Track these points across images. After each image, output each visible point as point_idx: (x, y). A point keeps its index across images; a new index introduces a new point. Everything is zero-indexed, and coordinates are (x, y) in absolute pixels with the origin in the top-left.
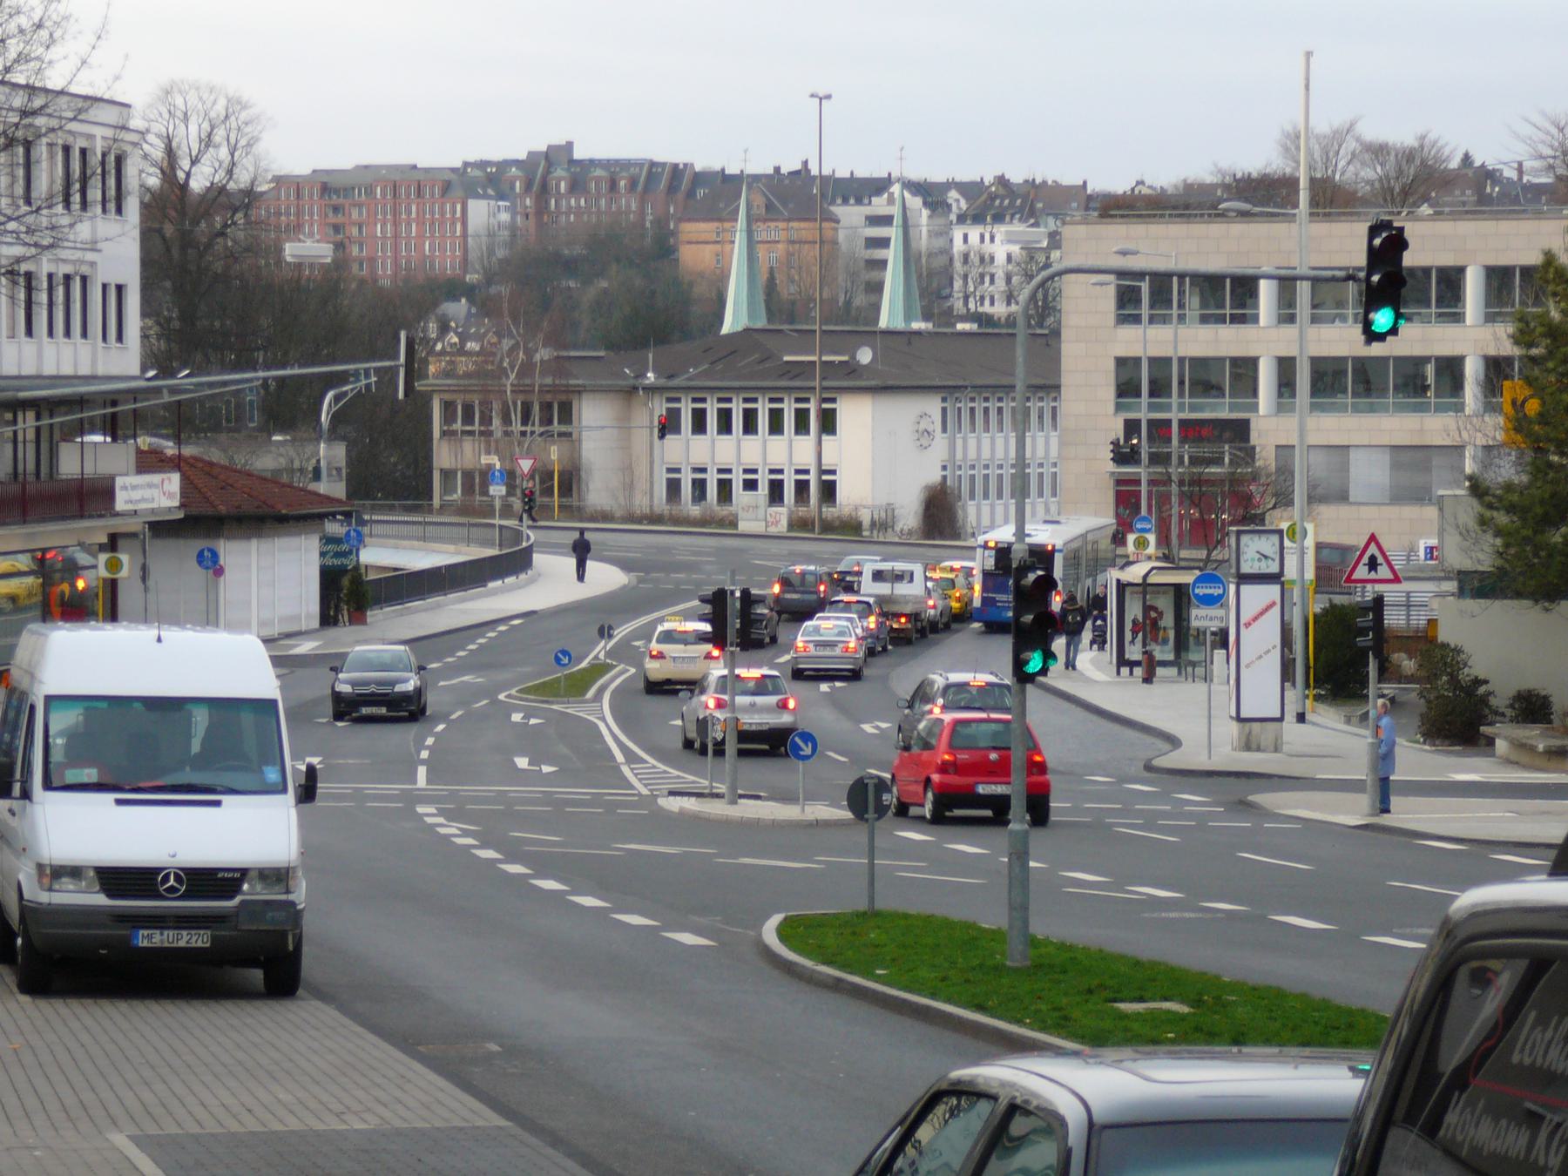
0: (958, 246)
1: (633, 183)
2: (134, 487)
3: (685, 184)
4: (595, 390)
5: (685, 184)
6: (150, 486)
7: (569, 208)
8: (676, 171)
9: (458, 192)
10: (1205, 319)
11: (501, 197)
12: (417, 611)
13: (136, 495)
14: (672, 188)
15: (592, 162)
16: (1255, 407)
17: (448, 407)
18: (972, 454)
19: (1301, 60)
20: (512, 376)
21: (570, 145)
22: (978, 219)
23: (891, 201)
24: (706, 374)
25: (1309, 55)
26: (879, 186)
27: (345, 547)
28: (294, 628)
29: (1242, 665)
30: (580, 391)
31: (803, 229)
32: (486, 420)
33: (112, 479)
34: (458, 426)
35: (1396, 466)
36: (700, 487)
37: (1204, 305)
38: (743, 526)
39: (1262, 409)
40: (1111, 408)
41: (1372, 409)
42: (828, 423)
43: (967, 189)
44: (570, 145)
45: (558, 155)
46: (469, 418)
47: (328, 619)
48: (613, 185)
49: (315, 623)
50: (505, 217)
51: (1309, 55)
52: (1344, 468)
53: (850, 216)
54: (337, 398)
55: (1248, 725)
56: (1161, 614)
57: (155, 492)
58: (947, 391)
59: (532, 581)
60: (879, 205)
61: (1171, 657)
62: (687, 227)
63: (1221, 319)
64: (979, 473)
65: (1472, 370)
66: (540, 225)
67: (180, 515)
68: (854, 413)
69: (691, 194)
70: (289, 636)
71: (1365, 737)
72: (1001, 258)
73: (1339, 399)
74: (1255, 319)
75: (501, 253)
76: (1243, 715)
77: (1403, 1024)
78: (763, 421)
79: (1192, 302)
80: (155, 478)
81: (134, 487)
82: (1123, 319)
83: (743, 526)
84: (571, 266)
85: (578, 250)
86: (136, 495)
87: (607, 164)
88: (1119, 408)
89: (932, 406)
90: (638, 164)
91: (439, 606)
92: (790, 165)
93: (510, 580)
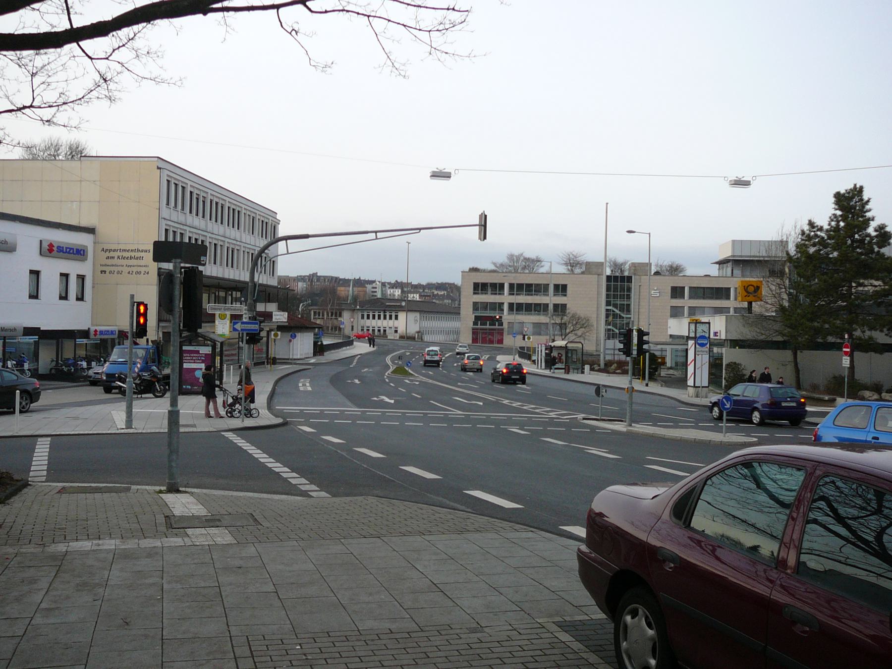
0: (389, 293)
1: (328, 280)
2: (277, 315)
3: (338, 281)
4: (347, 310)
5: (338, 281)
6: (281, 315)
7: (317, 285)
8: (336, 278)
9: (296, 281)
10: (492, 294)
11: (304, 282)
12: (334, 353)
13: (278, 317)
14: (335, 281)
15: (321, 276)
16: (503, 314)
17: (315, 313)
18: (423, 325)
19: (605, 204)
20: (329, 306)
21: (317, 273)
22: (393, 288)
23: (376, 284)
24: (370, 307)
25: (607, 204)
26: (374, 282)
27: (318, 336)
28: (307, 356)
29: (697, 368)
30: (343, 310)
31: (360, 289)
32: (323, 315)
33: (272, 312)
34: (317, 317)
35: (533, 327)
36: (379, 331)
37: (492, 291)
38: (389, 337)
39: (505, 314)
40: (472, 313)
41: (529, 314)
42: (396, 318)
43: (389, 283)
44: (317, 273)
45: (315, 275)
46: (319, 315)
47: (315, 354)
48: (325, 281)
49: (312, 355)
50: (305, 286)
51: (607, 204)
52: (523, 327)
53: (369, 287)
54: (303, 305)
55: (697, 389)
56: (562, 355)
57: (282, 317)
58: (420, 311)
59: (354, 347)
60: (374, 285)
61: (564, 367)
62: (339, 288)
63: (496, 294)
64: (440, 329)
65: (551, 307)
66: (311, 288)
67: (287, 324)
68: (402, 316)
69: (339, 282)
70: (307, 358)
71: (721, 394)
72: (397, 295)
73: (521, 312)
74: (504, 294)
75: (304, 292)
76: (696, 385)
77: (52, 385)
78: (377, 317)
79: (489, 290)
80: (282, 313)
81: (277, 315)
82: (474, 293)
83: (389, 337)
84: (317, 295)
85: (318, 292)
86: (278, 317)
87: (324, 276)
88: (473, 313)
89: (418, 315)
90: (330, 277)
91: (338, 352)
92: (357, 278)
93: (348, 347)
